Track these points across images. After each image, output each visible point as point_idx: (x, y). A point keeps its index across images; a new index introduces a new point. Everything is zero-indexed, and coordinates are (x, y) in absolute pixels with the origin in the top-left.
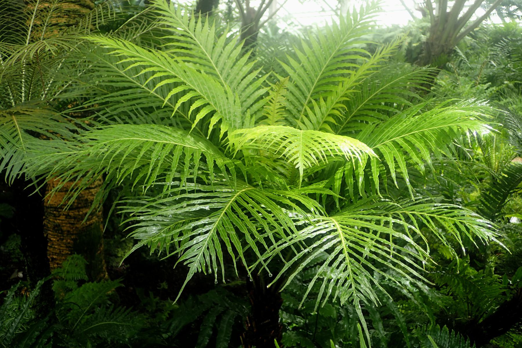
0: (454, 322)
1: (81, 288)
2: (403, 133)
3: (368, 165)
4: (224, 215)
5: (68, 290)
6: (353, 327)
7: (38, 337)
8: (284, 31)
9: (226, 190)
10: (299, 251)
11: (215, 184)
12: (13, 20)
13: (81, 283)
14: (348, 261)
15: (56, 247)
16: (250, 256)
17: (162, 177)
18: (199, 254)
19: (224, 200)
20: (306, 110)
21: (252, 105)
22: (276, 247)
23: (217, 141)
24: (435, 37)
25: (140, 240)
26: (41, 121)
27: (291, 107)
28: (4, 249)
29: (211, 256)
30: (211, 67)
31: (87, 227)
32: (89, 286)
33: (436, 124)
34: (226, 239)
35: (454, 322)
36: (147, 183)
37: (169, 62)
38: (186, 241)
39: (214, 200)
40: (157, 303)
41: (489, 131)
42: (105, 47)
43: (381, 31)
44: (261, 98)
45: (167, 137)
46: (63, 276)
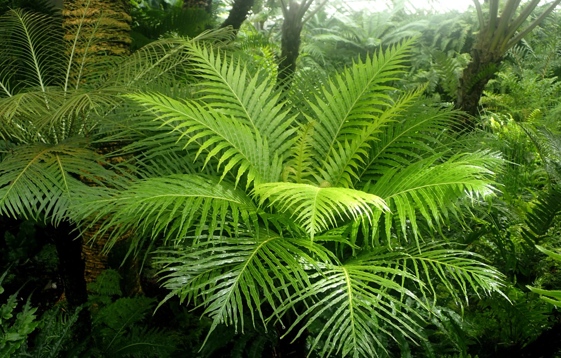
0: (496, 347)
1: (115, 304)
2: (417, 185)
4: (245, 269)
5: (102, 305)
8: (332, 17)
9: (249, 243)
10: (311, 304)
11: (240, 236)
13: (115, 298)
15: (91, 261)
16: (267, 309)
17: (192, 231)
18: (223, 306)
19: (246, 253)
21: (280, 146)
22: (290, 301)
23: (244, 189)
24: (484, 44)
25: (171, 291)
27: (318, 147)
28: (39, 259)
29: (232, 309)
30: (242, 111)
31: (121, 241)
32: (124, 301)
33: (446, 180)
34: (246, 293)
35: (496, 347)
36: (178, 238)
38: (210, 295)
40: (191, 319)
41: (492, 192)
43: (436, 20)
45: (197, 189)
46: (98, 291)
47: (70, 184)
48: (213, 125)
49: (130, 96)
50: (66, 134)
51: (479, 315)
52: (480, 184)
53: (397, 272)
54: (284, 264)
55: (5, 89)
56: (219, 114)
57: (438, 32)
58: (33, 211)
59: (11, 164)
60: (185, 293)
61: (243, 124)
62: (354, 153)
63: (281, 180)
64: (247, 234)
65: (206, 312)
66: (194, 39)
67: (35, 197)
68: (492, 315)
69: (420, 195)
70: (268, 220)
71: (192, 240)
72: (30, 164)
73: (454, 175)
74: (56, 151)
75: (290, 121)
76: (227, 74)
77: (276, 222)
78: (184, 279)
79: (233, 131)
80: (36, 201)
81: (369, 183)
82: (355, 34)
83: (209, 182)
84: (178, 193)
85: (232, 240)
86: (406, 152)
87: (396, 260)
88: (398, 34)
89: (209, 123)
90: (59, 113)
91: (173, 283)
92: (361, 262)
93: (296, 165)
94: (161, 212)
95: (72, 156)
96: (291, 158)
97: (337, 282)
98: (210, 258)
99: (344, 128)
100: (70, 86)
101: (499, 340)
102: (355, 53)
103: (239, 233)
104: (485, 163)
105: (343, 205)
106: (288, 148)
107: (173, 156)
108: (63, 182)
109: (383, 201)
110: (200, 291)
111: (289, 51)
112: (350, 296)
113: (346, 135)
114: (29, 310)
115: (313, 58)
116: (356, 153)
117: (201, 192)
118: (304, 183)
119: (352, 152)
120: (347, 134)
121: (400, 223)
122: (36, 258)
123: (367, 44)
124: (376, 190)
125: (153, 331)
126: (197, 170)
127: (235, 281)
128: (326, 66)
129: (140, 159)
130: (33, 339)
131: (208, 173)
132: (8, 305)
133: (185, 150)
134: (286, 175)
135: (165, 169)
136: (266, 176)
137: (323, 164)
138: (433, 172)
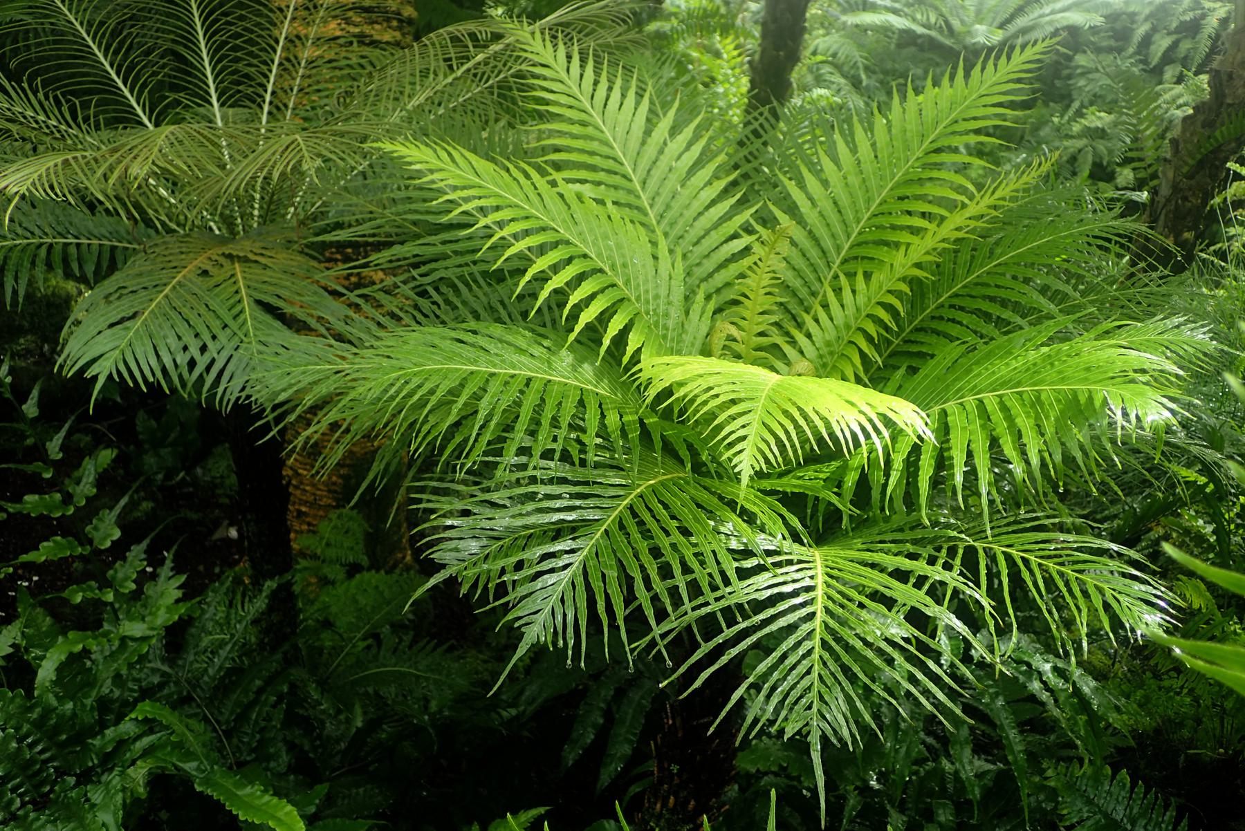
2: (1004, 385)
3: (916, 450)
4: (601, 536)
5: (325, 582)
6: (904, 749)
7: (260, 691)
9: (618, 481)
10: (731, 623)
11: (597, 466)
12: (245, 29)
13: (353, 570)
14: (817, 656)
15: (308, 488)
16: (637, 623)
18: (545, 608)
19: (606, 503)
20: (825, 296)
21: (711, 275)
22: (689, 611)
25: (443, 566)
26: (288, 284)
27: (797, 283)
28: (204, 474)
29: (565, 615)
30: (630, 192)
32: (372, 578)
34: (597, 585)
36: (466, 457)
37: (539, 195)
39: (588, 501)
41: (1168, 414)
42: (413, 167)
44: (735, 258)
45: (516, 358)
46: (319, 551)
47: (258, 325)
48: (564, 221)
49: (388, 147)
50: (260, 216)
51: (1153, 684)
52: (1142, 394)
53: (936, 573)
54: (686, 532)
55: (139, 111)
56: (580, 197)
57: (1146, 19)
58: (180, 376)
59: (140, 275)
60: (472, 573)
61: (632, 222)
62: (873, 301)
63: (706, 352)
64: (614, 463)
65: (510, 617)
66: (538, 24)
67: (185, 348)
68: (1182, 687)
69: (1005, 409)
70: (662, 436)
71: (495, 465)
72: (179, 277)
73: (1088, 369)
74: (235, 253)
75: (739, 220)
76: (606, 105)
77: (678, 439)
78: (473, 546)
79: (606, 237)
80: (187, 358)
81: (902, 371)
82: (942, 15)
83: (546, 343)
84: (475, 362)
85: (581, 474)
86: (995, 310)
87: (939, 548)
88: (1048, 18)
89: (553, 215)
90: (240, 173)
91: (451, 550)
92: (858, 543)
93: (744, 319)
94: (434, 400)
95: (265, 267)
96: (735, 303)
97: (794, 581)
98: (530, 507)
99: (859, 245)
100: (275, 111)
101: (1191, 744)
102: (938, 60)
103: (596, 459)
104: (1166, 348)
105: (823, 418)
106: (728, 280)
107: (475, 281)
108: (245, 321)
109: (923, 414)
110: (503, 571)
111: (778, 51)
112: (819, 614)
113: (860, 260)
114: (170, 578)
115: (838, 67)
116: (878, 303)
117: (524, 365)
118: (754, 362)
119: (869, 299)
120: (863, 258)
121: (952, 466)
122: (199, 471)
123: (970, 41)
124: (914, 390)
125: (424, 648)
126: (525, 315)
127: (577, 559)
128: (867, 87)
129: (405, 282)
130: (176, 637)
131: (549, 324)
132: (127, 565)
133: (500, 270)
134: (718, 341)
135: (457, 308)
136: (672, 340)
137: (804, 323)
138: (1044, 360)
